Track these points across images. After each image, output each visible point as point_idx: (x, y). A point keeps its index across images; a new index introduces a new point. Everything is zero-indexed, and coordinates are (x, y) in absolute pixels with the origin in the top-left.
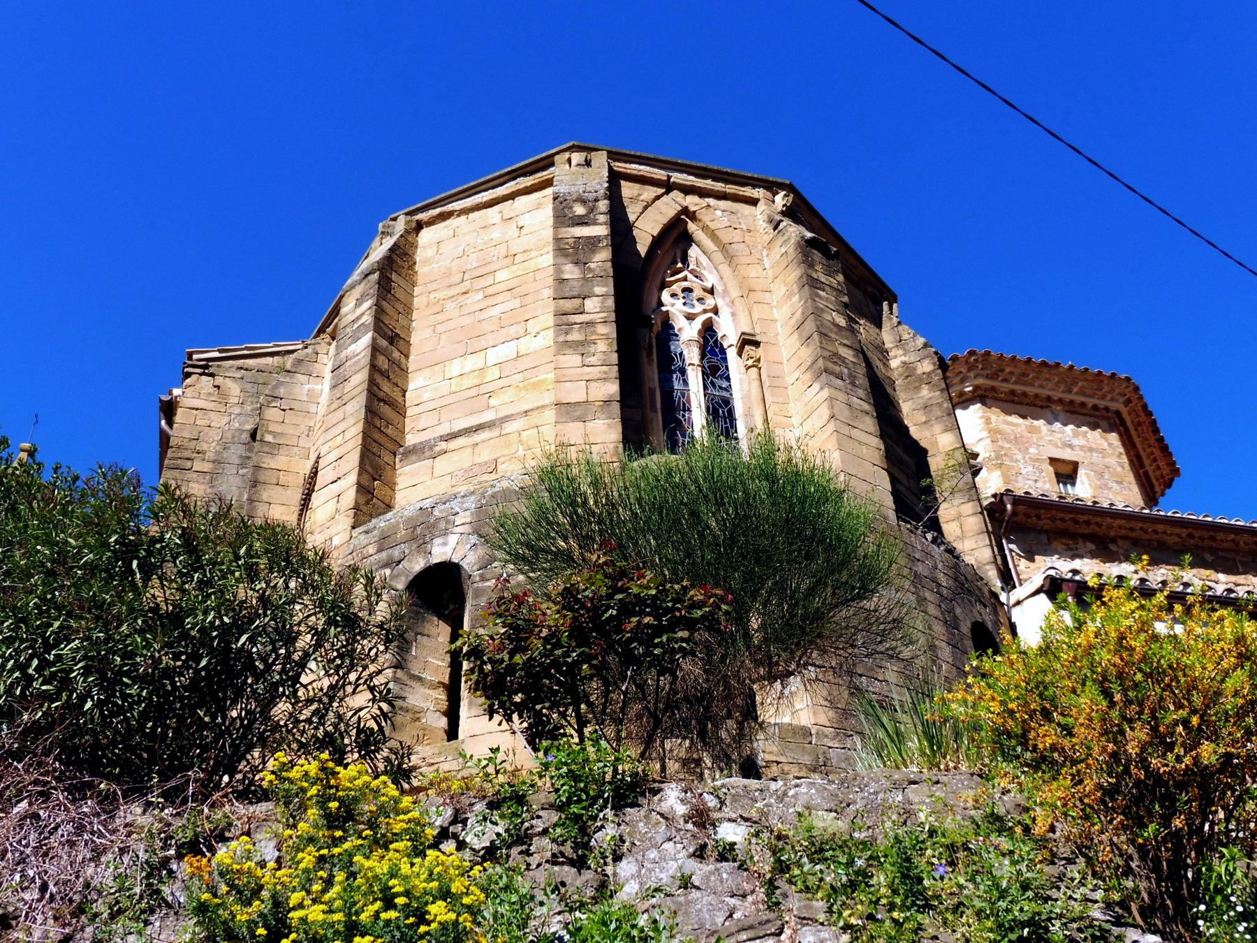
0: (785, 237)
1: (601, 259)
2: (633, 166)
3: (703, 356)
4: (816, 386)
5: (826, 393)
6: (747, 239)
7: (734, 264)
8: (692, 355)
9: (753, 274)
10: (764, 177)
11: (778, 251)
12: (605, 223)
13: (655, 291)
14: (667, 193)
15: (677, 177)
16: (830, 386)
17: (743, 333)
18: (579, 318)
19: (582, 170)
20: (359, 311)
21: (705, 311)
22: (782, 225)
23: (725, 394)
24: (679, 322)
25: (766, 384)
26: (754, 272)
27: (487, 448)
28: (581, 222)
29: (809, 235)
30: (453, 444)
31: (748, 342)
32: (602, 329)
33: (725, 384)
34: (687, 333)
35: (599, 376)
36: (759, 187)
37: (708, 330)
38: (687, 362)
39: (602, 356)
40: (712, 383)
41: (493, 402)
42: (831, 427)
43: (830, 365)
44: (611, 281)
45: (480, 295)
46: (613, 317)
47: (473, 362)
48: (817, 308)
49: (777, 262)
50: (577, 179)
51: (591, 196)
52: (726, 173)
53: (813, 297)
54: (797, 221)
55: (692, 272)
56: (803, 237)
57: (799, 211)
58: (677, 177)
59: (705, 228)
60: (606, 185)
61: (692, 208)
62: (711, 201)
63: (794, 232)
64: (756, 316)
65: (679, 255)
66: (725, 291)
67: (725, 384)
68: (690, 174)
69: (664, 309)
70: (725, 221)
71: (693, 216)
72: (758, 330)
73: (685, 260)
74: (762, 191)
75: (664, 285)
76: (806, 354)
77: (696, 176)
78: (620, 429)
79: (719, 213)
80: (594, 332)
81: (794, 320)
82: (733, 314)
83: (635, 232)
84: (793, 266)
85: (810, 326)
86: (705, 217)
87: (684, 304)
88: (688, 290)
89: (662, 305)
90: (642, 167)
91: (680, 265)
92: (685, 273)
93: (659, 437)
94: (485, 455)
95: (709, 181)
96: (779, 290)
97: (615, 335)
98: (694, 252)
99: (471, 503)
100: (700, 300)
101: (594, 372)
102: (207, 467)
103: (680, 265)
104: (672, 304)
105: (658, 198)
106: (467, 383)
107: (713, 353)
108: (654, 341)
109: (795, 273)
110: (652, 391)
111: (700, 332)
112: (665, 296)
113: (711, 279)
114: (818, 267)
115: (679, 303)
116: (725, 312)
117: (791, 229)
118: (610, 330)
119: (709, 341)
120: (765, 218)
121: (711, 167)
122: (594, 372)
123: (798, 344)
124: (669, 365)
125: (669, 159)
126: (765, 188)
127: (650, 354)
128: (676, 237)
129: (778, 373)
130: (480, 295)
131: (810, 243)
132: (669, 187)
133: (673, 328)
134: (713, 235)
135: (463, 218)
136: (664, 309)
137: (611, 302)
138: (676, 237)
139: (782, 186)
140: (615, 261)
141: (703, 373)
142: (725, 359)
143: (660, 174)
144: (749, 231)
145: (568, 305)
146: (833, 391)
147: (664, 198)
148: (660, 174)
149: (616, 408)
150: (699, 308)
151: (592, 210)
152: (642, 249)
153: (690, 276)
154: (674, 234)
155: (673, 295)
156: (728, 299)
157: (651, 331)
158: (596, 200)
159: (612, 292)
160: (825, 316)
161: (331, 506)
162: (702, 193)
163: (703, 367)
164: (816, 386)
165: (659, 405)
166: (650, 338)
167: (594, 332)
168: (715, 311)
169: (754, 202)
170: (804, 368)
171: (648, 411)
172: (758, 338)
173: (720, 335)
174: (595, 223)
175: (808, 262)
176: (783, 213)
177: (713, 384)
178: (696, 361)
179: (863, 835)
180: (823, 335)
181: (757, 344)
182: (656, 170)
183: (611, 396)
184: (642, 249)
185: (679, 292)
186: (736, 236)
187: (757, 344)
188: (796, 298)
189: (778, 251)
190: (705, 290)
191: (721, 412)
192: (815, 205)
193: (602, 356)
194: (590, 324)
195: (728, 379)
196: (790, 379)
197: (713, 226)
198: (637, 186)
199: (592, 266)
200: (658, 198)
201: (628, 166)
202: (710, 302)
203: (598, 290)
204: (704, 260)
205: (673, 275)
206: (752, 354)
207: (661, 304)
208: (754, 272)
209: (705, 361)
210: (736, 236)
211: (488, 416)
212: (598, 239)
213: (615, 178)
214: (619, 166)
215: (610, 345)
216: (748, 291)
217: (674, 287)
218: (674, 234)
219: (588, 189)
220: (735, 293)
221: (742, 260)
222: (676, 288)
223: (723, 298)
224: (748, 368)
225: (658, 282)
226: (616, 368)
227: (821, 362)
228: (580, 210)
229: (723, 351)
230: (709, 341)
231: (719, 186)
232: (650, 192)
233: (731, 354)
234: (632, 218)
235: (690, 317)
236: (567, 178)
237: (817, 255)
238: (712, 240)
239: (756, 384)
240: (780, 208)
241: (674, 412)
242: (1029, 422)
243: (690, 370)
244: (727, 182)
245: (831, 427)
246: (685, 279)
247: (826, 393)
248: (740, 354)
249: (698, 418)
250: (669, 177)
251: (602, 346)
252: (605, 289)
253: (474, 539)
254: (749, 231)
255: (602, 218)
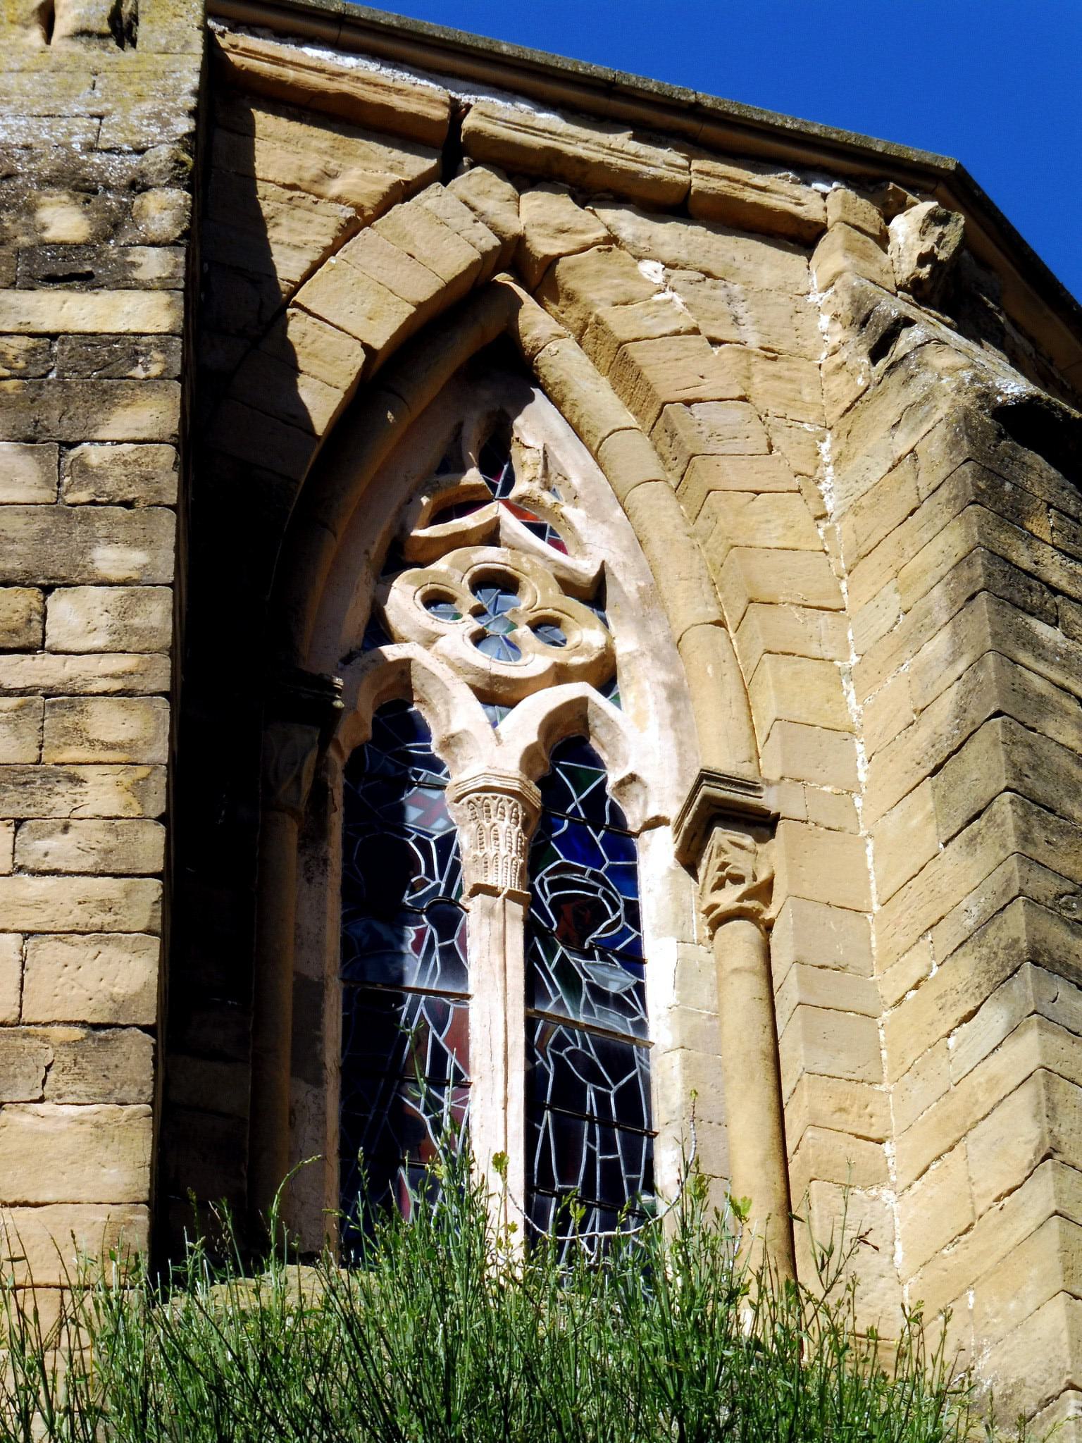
0: (914, 392)
1: (144, 419)
2: (311, 54)
3: (535, 856)
4: (994, 1019)
5: (1029, 1049)
6: (758, 386)
7: (695, 489)
8: (491, 852)
9: (772, 536)
10: (850, 135)
11: (880, 444)
12: (164, 285)
13: (363, 575)
14: (446, 174)
15: (492, 115)
16: (1048, 1021)
17: (707, 776)
19: (95, 55)
21: (561, 674)
22: (907, 339)
23: (614, 1021)
24: (452, 713)
25: (787, 999)
26: (774, 524)
28: (70, 270)
29: (1014, 386)
31: (724, 812)
32: (110, 723)
33: (617, 981)
34: (482, 753)
35: (79, 917)
36: (829, 175)
37: (568, 751)
38: (469, 877)
39: (99, 835)
40: (565, 971)
42: (1041, 1194)
43: (1058, 935)
44: (167, 524)
46: (160, 675)
48: (1025, 694)
49: (877, 491)
50: (68, 92)
51: (117, 168)
52: (695, 110)
53: (1009, 646)
54: (975, 325)
55: (517, 508)
56: (985, 397)
57: (978, 286)
58: (492, 115)
59: (588, 332)
60: (185, 125)
61: (542, 246)
62: (626, 222)
63: (957, 369)
64: (767, 706)
65: (473, 435)
66: (652, 597)
67: (617, 981)
68: (543, 103)
69: (391, 652)
70: (676, 308)
71: (543, 279)
72: (771, 769)
73: (496, 457)
74: (838, 193)
75: (400, 556)
76: (967, 878)
77: (571, 112)
78: (141, 1146)
79: (651, 270)
80: (77, 734)
81: (922, 735)
82: (675, 694)
83: (297, 328)
84: (937, 510)
85: (984, 767)
86: (592, 283)
87: (479, 638)
88: (498, 583)
89: (388, 637)
90: (349, 62)
91: (473, 477)
92: (495, 510)
93: (315, 1160)
95: (621, 139)
96: (875, 605)
97: (160, 752)
98: (535, 426)
100: (544, 625)
101: (61, 900)
103: (473, 477)
104: (432, 642)
105: (405, 192)
107: (578, 846)
108: (337, 783)
109: (944, 542)
110: (310, 993)
111: (530, 757)
112: (403, 599)
113: (595, 545)
114: (1042, 525)
115: (455, 635)
116: (642, 685)
117: (943, 360)
118: (144, 729)
119: (568, 793)
120: (843, 304)
121: (632, 79)
122: (61, 900)
123: (931, 838)
124: (395, 884)
125: (463, 36)
126: (850, 181)
127: (314, 835)
128: (468, 358)
129: (839, 953)
131: (1016, 421)
132: (451, 150)
133: (422, 733)
134: (620, 364)
136: (391, 652)
137: (157, 614)
138: (468, 358)
139: (922, 179)
140: (195, 442)
141: (531, 929)
142: (628, 877)
143: (420, 95)
144: (771, 354)
146: (1059, 1041)
147: (432, 197)
148: (420, 95)
149: (135, 1058)
150: (536, 659)
151: (113, 226)
152: (321, 398)
153: (513, 526)
154: (462, 346)
155: (435, 599)
156: (658, 632)
157: (327, 739)
158: (137, 186)
159: (166, 572)
160: (1050, 727)
162: (590, 186)
163: (533, 902)
164: (994, 1019)
165: (332, 1054)
166: (322, 765)
167: (77, 734)
168: (605, 675)
169: (801, 237)
170: (948, 936)
171: (284, 1075)
172: (769, 800)
173: (613, 776)
174: (124, 282)
175: (992, 495)
176: (917, 290)
177: (568, 976)
178: (505, 876)
180: (1035, 806)
181: (762, 824)
182: (404, 79)
183: (121, 1004)
184: (321, 398)
185: (460, 587)
186: (716, 372)
187: (762, 824)
188: (939, 644)
189: (880, 444)
190: (568, 586)
191: (590, 1108)
193: (99, 835)
194: (65, 697)
195: (633, 960)
196: (891, 982)
197: (621, 323)
198: (322, 138)
199: (95, 455)
200: (405, 192)
201: (288, 51)
202: (586, 637)
203: (111, 559)
204: (574, 462)
205: (441, 516)
206: (741, 862)
207: (379, 631)
208: (774, 524)
209: (544, 876)
210: (716, 372)
212: (128, 346)
213: (227, 100)
214: (254, 51)
215: (139, 789)
216: (741, 607)
217: (442, 565)
218: (462, 346)
219: (109, 137)
220: (689, 606)
221: (733, 474)
222: (450, 570)
223: (642, 625)
224: (719, 920)
225: (376, 543)
226: (153, 889)
227: (1017, 922)
228: (64, 221)
229: (623, 844)
230: (568, 793)
231: (662, 163)
232: (370, 167)
233: (656, 857)
234: (288, 266)
235: (497, 695)
236: (28, 82)
237: (1038, 474)
238: (617, 383)
239: (746, 989)
240: (907, 268)
241: (391, 1122)
242: (407, 315)
243: (475, 912)
244: (696, 146)
245: (1041, 1194)
246: (491, 536)
247: (1029, 1049)
248: (690, 858)
249: (493, 1116)
250: (457, 111)
251: (103, 793)
252: (138, 557)
254: (771, 354)
255: (154, 263)
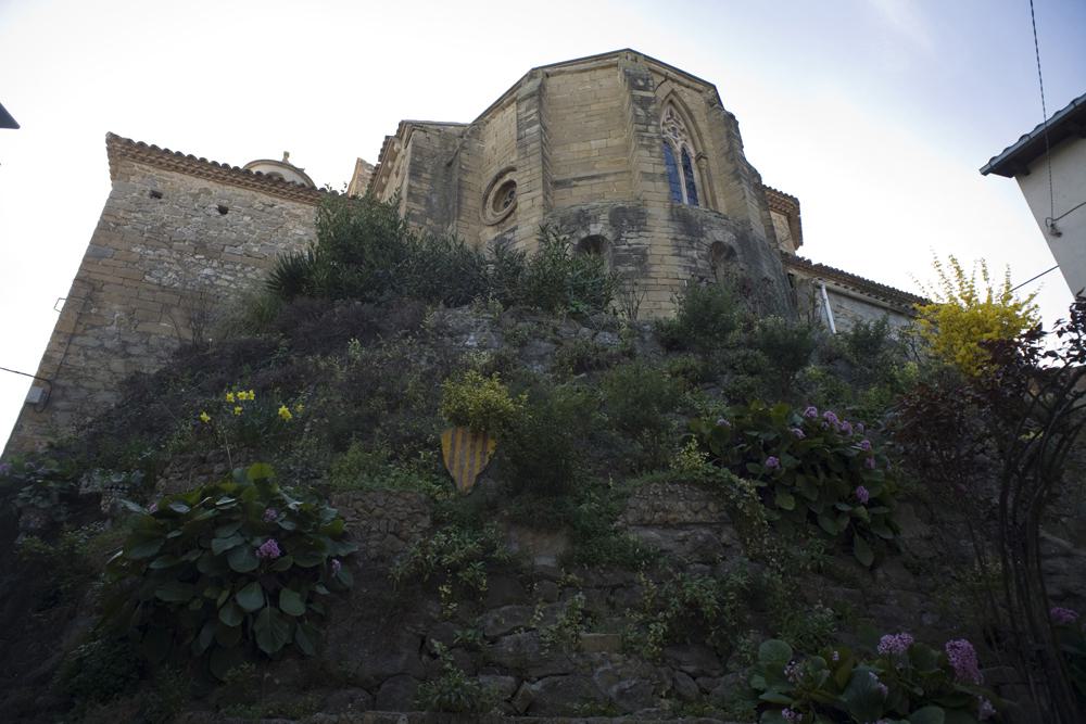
18: (647, 134)
20: (529, 113)
27: (597, 187)
30: (580, 183)
41: (597, 166)
45: (584, 115)
47: (583, 146)
94: (597, 190)
99: (607, 210)
102: (428, 176)
106: (582, 156)
130: (584, 115)
135: (569, 76)
145: (641, 127)
161: (529, 203)
179: (689, 398)
192: (510, 87)
194: (652, 138)
211: (595, 173)
228: (641, 83)
253: (610, 227)
